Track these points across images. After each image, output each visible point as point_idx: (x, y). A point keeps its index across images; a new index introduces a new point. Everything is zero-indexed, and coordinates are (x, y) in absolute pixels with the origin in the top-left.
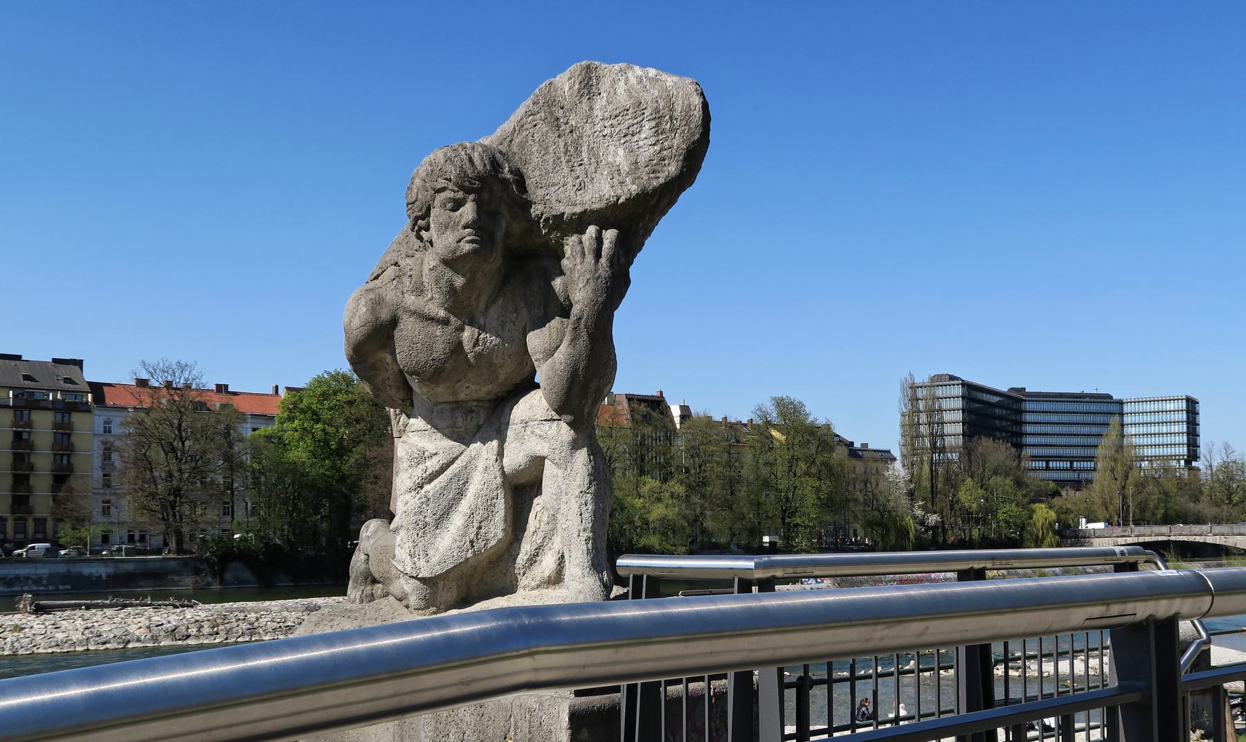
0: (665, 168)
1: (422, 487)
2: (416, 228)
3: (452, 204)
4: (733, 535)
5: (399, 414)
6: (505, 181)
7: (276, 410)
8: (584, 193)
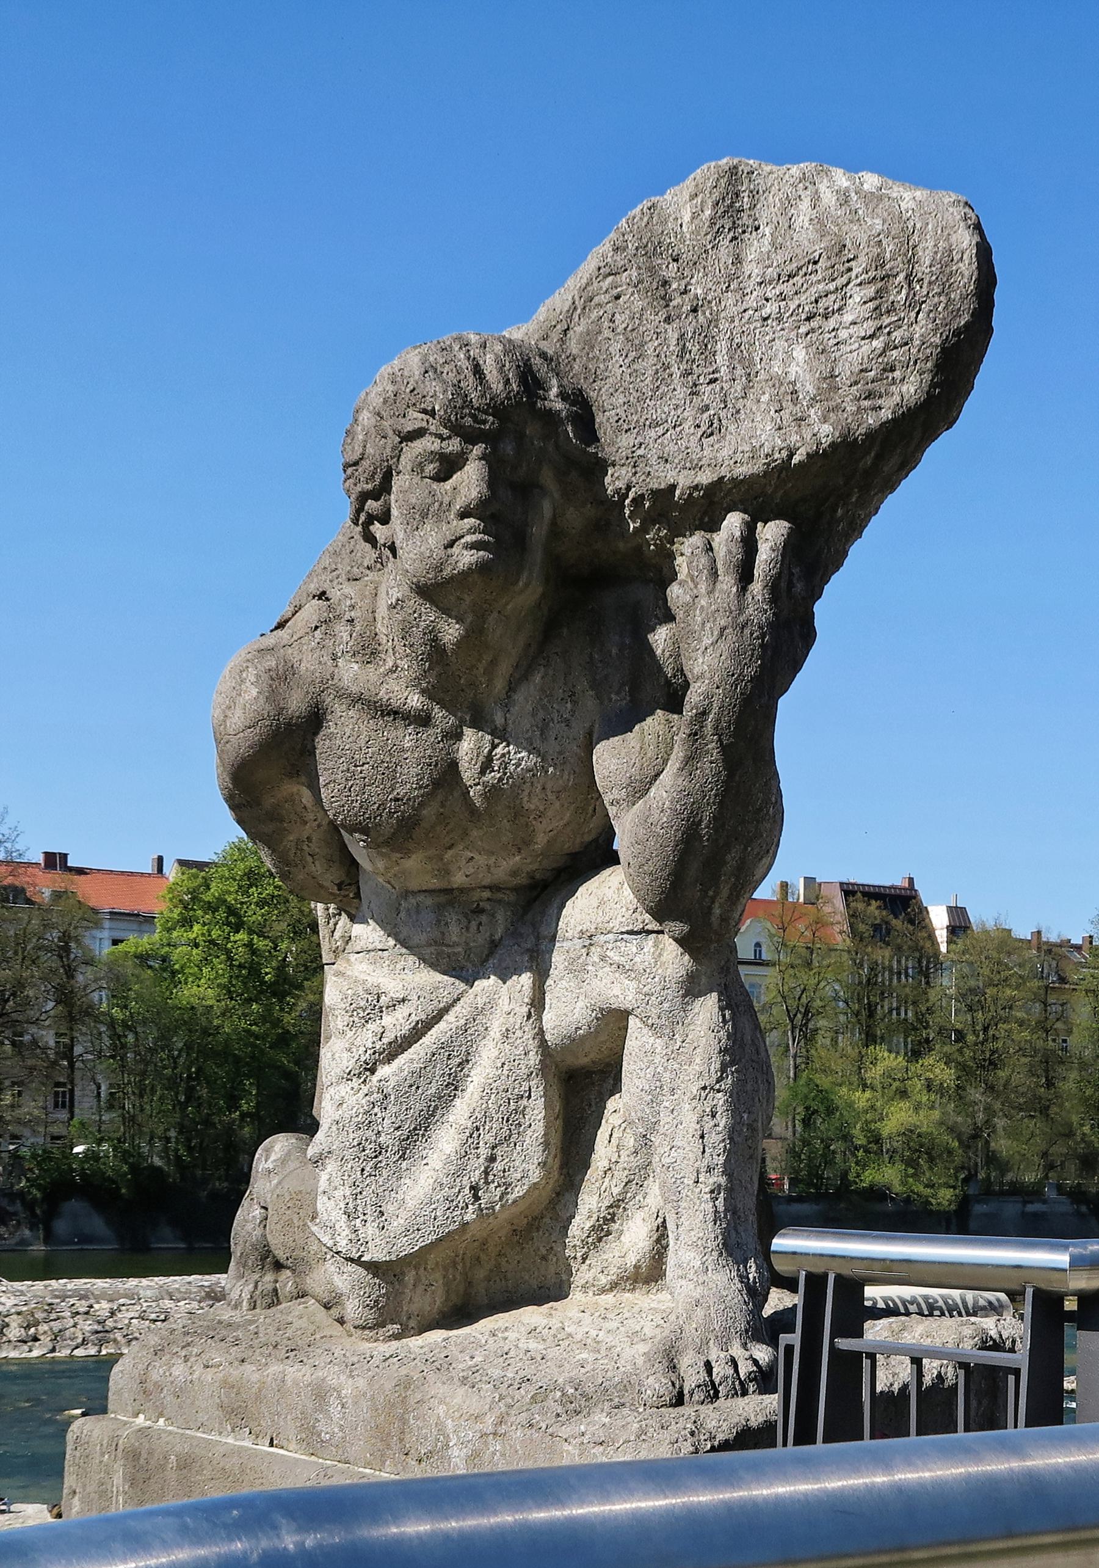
0: (894, 387)
1: (373, 1071)
2: (362, 518)
3: (438, 464)
4: (1050, 1167)
5: (334, 915)
6: (550, 416)
7: (161, 906)
8: (719, 441)
